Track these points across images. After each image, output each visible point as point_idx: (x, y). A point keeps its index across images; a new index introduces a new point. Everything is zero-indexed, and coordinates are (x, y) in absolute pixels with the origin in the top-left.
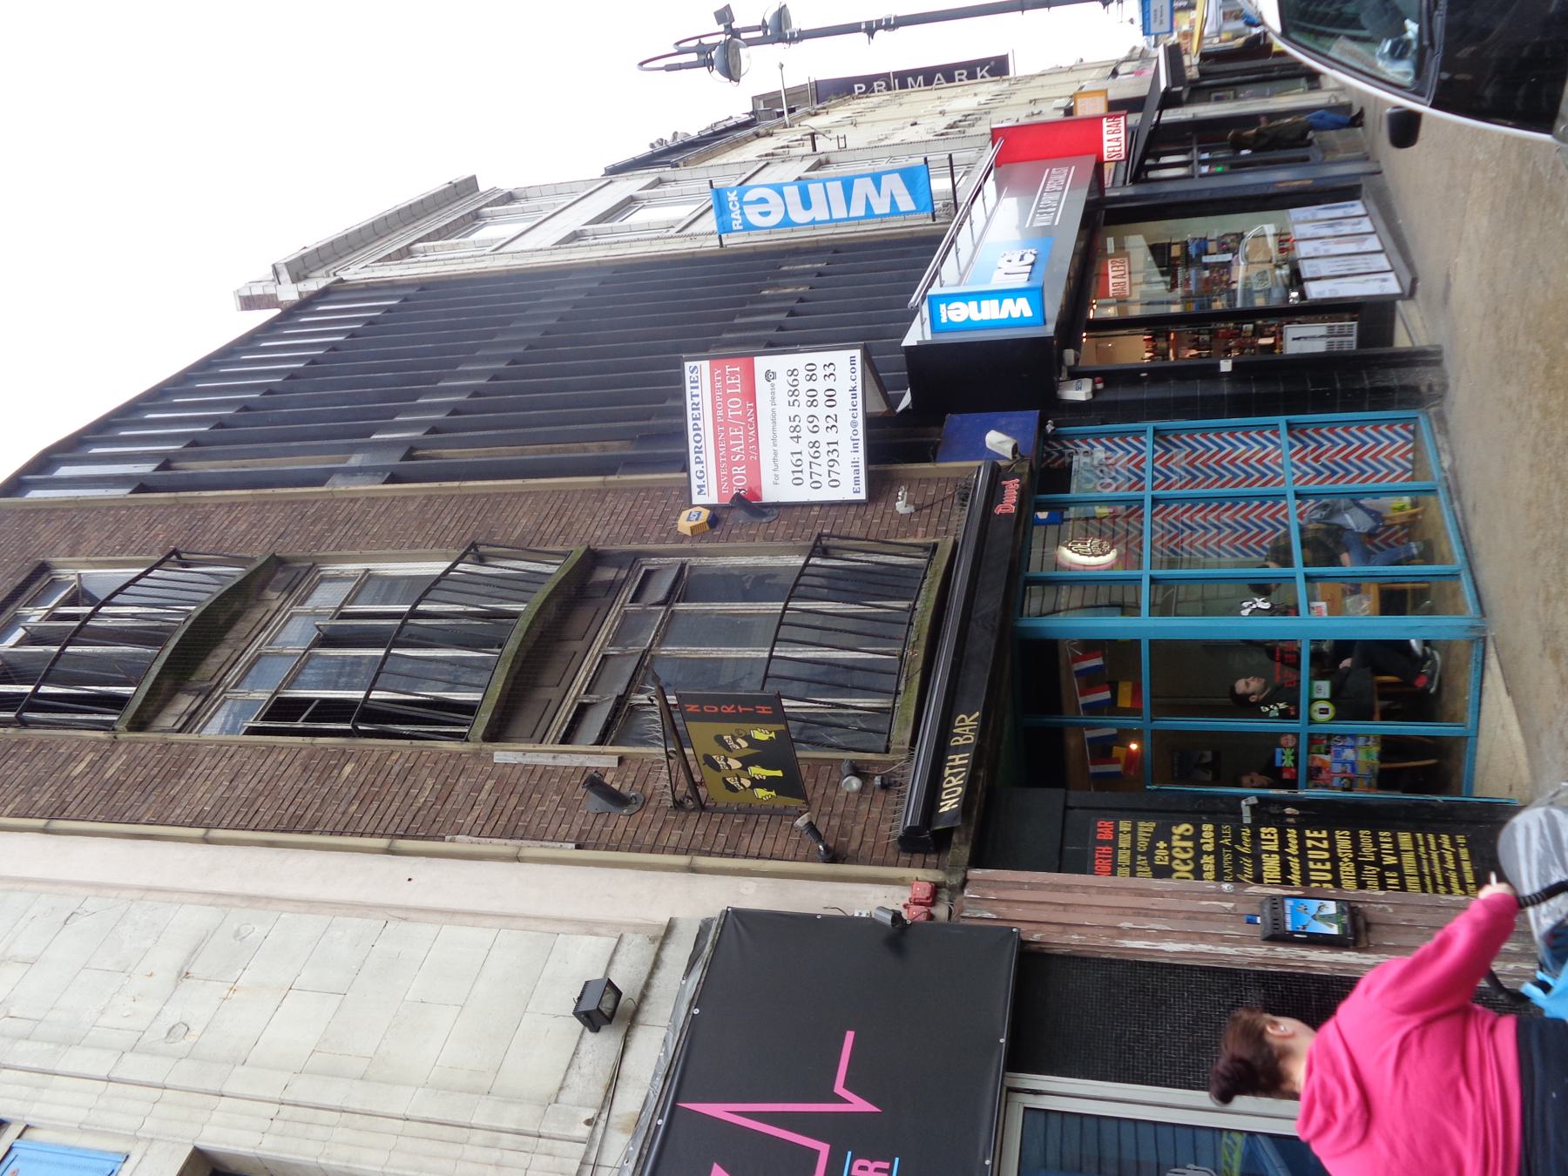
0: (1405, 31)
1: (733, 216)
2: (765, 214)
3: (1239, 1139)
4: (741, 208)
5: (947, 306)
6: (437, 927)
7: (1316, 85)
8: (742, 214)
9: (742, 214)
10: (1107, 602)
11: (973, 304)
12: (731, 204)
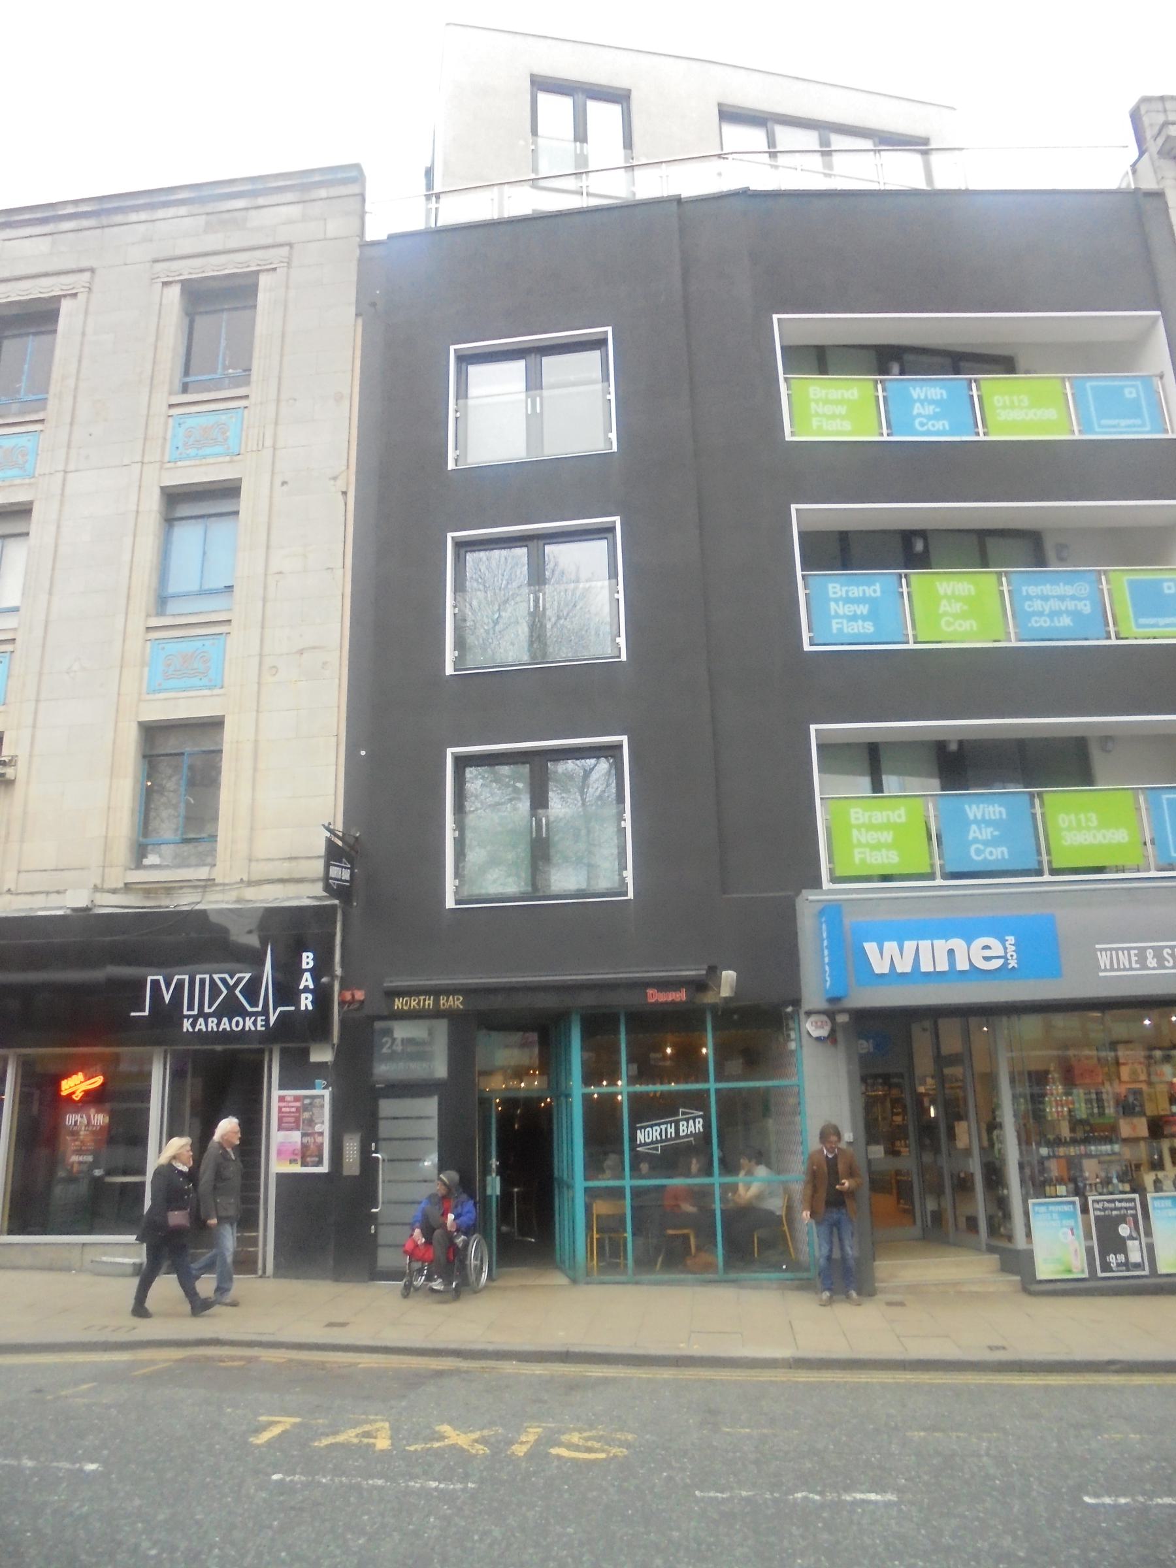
0: (30, 1458)
1: (1013, 948)
2: (987, 947)
3: (625, 889)
4: (1006, 953)
5: (1006, 964)
6: (439, 224)
7: (50, 328)
8: (1005, 949)
9: (1005, 949)
10: (195, 587)
11: (962, 965)
12: (1015, 957)
